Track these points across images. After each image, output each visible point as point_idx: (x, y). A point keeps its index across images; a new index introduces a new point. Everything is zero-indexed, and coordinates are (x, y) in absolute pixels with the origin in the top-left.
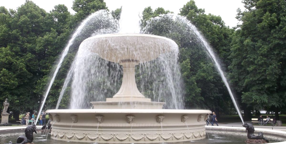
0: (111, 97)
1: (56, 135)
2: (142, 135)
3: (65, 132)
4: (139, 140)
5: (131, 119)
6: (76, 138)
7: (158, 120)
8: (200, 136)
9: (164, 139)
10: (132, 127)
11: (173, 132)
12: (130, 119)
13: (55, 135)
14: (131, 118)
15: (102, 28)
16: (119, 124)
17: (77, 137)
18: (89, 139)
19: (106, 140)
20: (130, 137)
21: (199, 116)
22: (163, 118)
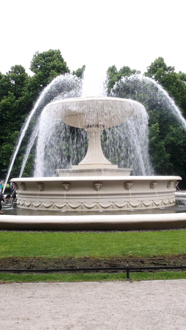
1: (22, 204)
2: (110, 202)
3: (32, 200)
5: (99, 187)
7: (126, 187)
8: (169, 203)
9: (133, 206)
10: (100, 195)
11: (141, 199)
12: (65, 187)
13: (21, 204)
16: (75, 191)
18: (56, 207)
19: (74, 208)
20: (82, 205)
21: (169, 182)
22: (131, 185)
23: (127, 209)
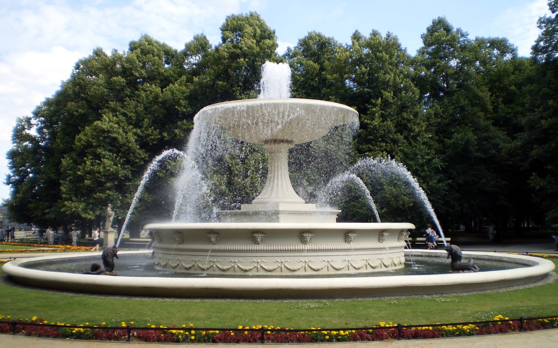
0: (249, 202)
1: (165, 263)
3: (168, 258)
4: (273, 270)
6: (182, 267)
7: (303, 239)
11: (329, 259)
14: (258, 236)
15: (382, 98)
16: (243, 245)
17: (183, 266)
21: (402, 231)
22: (311, 237)
23: (256, 274)
